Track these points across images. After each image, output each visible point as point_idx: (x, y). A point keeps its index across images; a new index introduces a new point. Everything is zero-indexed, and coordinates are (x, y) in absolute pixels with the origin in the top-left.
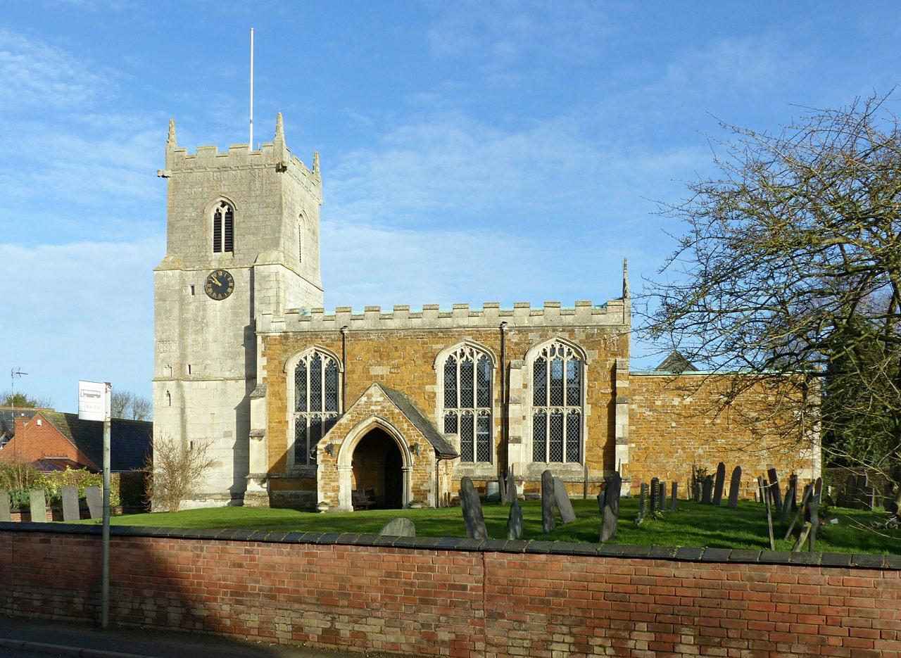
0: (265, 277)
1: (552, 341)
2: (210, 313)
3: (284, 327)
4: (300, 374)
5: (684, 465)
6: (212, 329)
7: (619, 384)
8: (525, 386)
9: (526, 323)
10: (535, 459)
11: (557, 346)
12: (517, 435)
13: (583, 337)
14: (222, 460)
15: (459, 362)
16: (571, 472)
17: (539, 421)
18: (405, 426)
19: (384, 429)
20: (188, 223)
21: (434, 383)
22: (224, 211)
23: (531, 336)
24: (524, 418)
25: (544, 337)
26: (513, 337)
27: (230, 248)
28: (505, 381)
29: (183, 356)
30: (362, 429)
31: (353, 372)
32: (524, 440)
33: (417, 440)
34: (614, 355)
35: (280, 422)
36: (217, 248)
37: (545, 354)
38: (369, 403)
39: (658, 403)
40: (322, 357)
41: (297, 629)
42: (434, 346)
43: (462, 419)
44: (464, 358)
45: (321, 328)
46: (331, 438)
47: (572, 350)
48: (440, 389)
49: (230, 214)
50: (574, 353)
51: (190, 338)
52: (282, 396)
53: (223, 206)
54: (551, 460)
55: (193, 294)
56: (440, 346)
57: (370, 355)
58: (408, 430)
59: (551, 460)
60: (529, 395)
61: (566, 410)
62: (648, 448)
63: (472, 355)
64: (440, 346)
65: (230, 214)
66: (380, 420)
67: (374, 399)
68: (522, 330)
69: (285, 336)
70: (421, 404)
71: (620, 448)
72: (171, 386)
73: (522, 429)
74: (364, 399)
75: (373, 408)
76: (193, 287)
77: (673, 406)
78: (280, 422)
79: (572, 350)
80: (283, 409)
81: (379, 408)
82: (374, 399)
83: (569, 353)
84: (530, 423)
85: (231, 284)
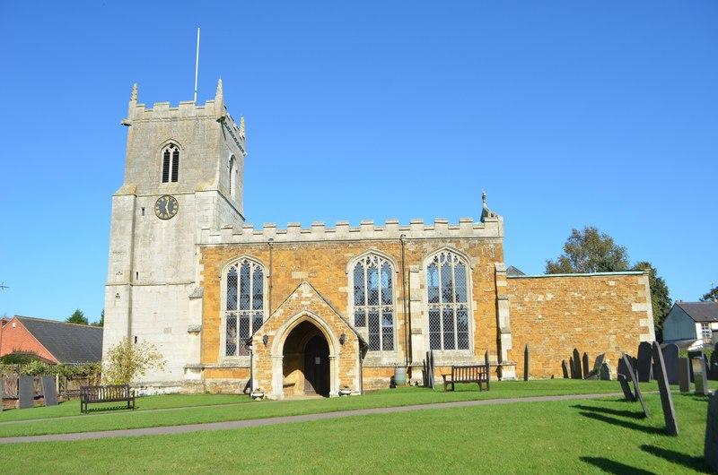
0: (205, 200)
1: (442, 251)
2: (157, 232)
3: (219, 240)
4: (232, 280)
5: (551, 350)
6: (158, 243)
7: (499, 283)
8: (422, 287)
9: (421, 236)
10: (432, 348)
11: (446, 254)
12: (417, 327)
13: (467, 246)
14: (579, 461)
15: (366, 267)
16: (463, 358)
17: (434, 316)
18: (332, 319)
19: (312, 321)
20: (143, 159)
21: (346, 285)
22: (172, 151)
23: (425, 245)
24: (422, 313)
25: (436, 248)
26: (410, 247)
27: (175, 179)
28: (404, 282)
29: (132, 266)
30: (293, 322)
31: (278, 277)
32: (423, 332)
33: (343, 331)
34: (493, 260)
35: (214, 319)
36: (165, 179)
37: (436, 260)
38: (299, 299)
39: (526, 299)
40: (251, 264)
41: (201, 273)
42: (346, 255)
43: (370, 315)
44: (370, 265)
45: (251, 240)
46: (265, 331)
47: (458, 257)
48: (350, 290)
49: (176, 153)
50: (459, 260)
51: (138, 251)
52: (216, 297)
53: (172, 147)
54: (445, 348)
55: (143, 214)
56: (350, 255)
57: (291, 262)
58: (335, 322)
59: (445, 348)
60: (425, 295)
61: (455, 306)
62: (521, 337)
63: (376, 261)
64: (350, 255)
65: (176, 153)
66: (309, 314)
67: (304, 295)
68: (419, 241)
69: (220, 247)
70: (336, 302)
71: (503, 337)
72: (122, 290)
73: (421, 323)
74: (295, 295)
75: (302, 303)
76: (143, 210)
77: (538, 302)
78: (214, 319)
79: (458, 257)
80: (217, 308)
81: (309, 303)
82: (304, 295)
83: (456, 260)
84: (427, 317)
85: (175, 207)
